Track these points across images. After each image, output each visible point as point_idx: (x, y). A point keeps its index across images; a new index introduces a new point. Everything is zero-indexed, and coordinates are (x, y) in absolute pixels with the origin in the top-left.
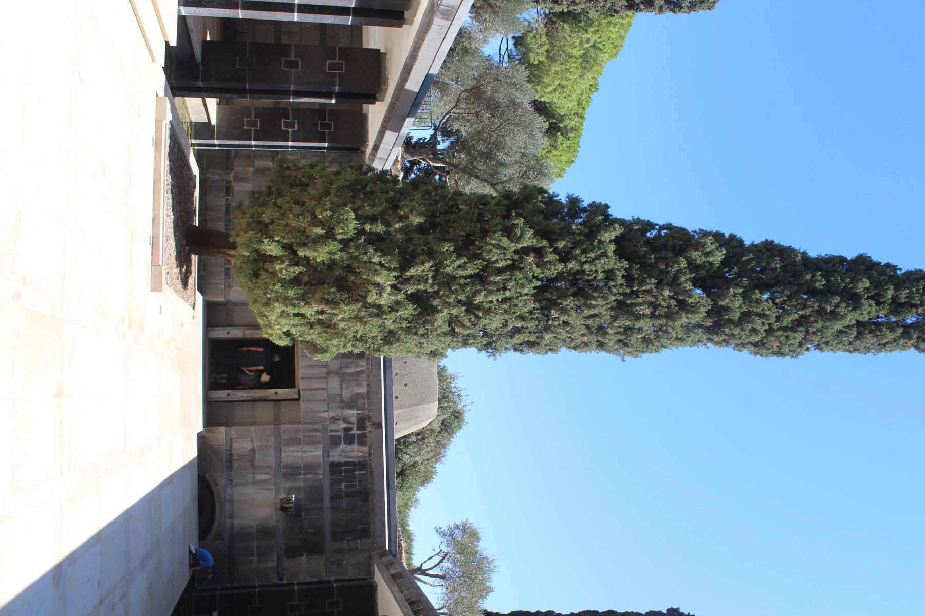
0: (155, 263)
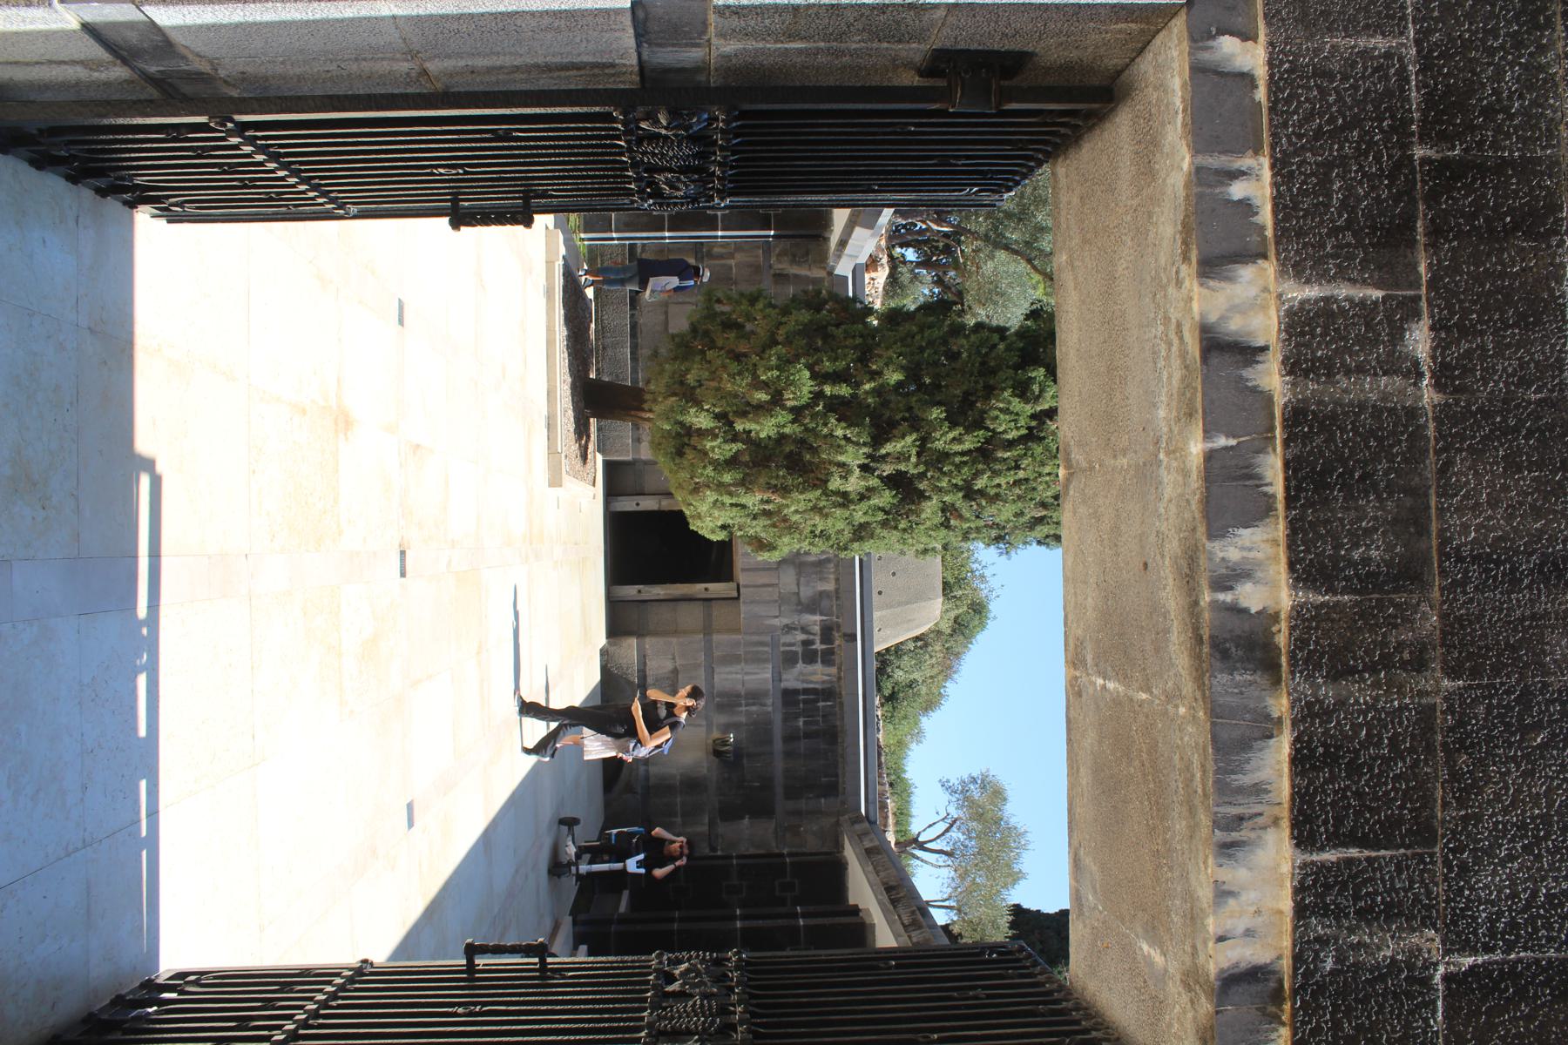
0: (552, 451)
